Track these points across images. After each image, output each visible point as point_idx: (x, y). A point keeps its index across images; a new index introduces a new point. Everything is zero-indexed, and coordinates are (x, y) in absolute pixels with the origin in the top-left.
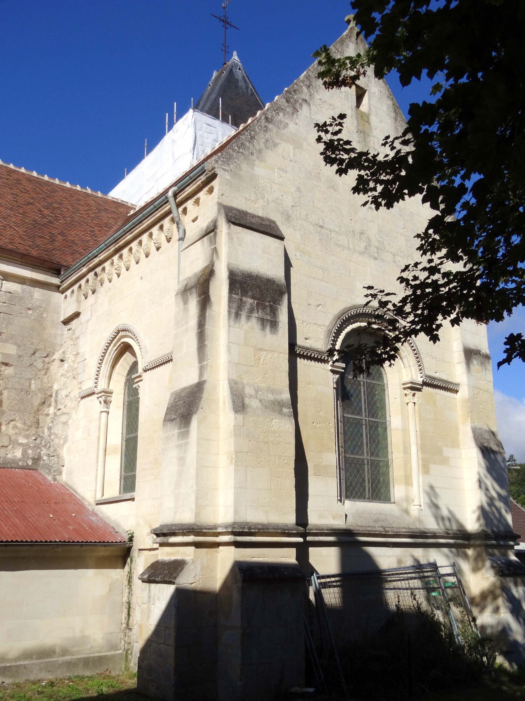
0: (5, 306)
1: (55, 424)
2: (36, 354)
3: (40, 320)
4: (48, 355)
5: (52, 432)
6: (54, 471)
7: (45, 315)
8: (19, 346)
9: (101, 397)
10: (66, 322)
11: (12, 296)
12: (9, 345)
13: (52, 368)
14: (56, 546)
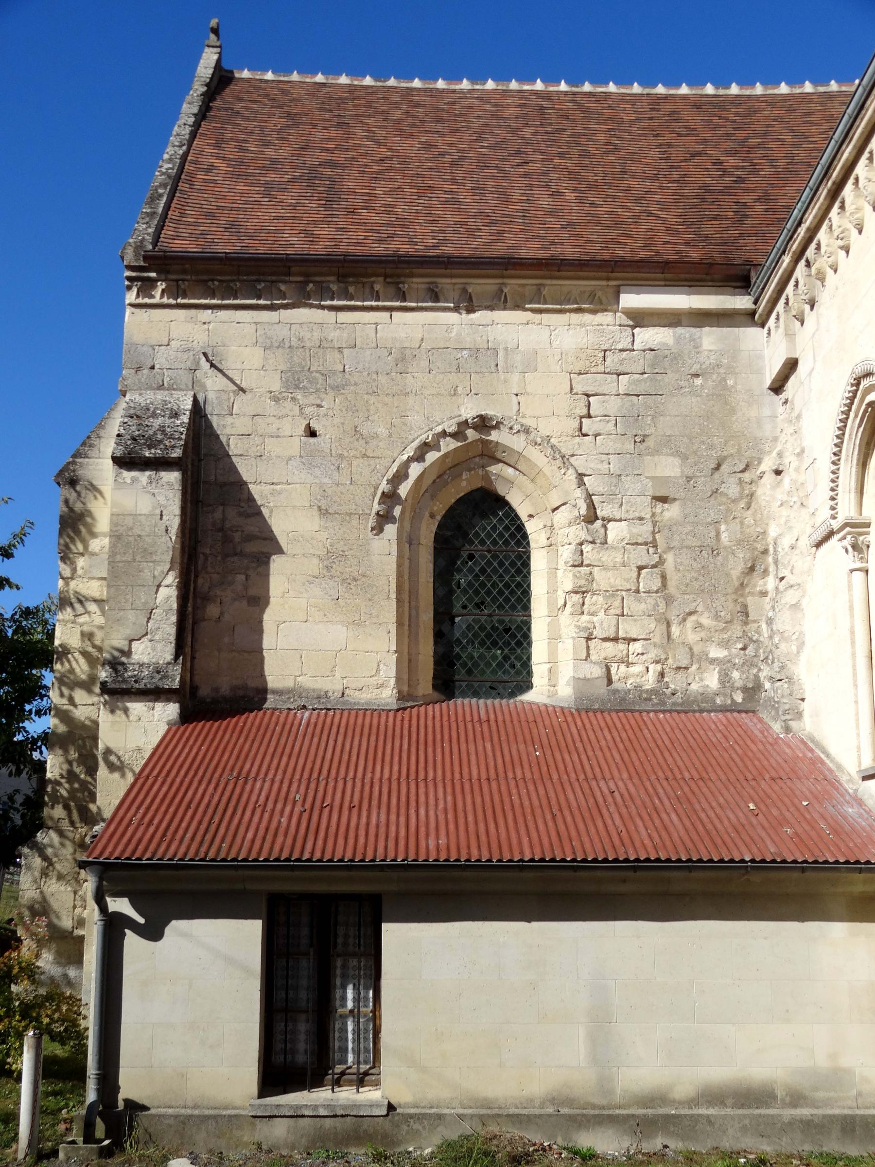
0: (645, 380)
1: (777, 610)
2: (723, 467)
3: (722, 394)
4: (747, 466)
5: (775, 629)
6: (785, 713)
7: (730, 382)
8: (684, 458)
9: (844, 538)
10: (777, 387)
11: (656, 356)
12: (663, 458)
13: (759, 492)
14: (743, 871)
